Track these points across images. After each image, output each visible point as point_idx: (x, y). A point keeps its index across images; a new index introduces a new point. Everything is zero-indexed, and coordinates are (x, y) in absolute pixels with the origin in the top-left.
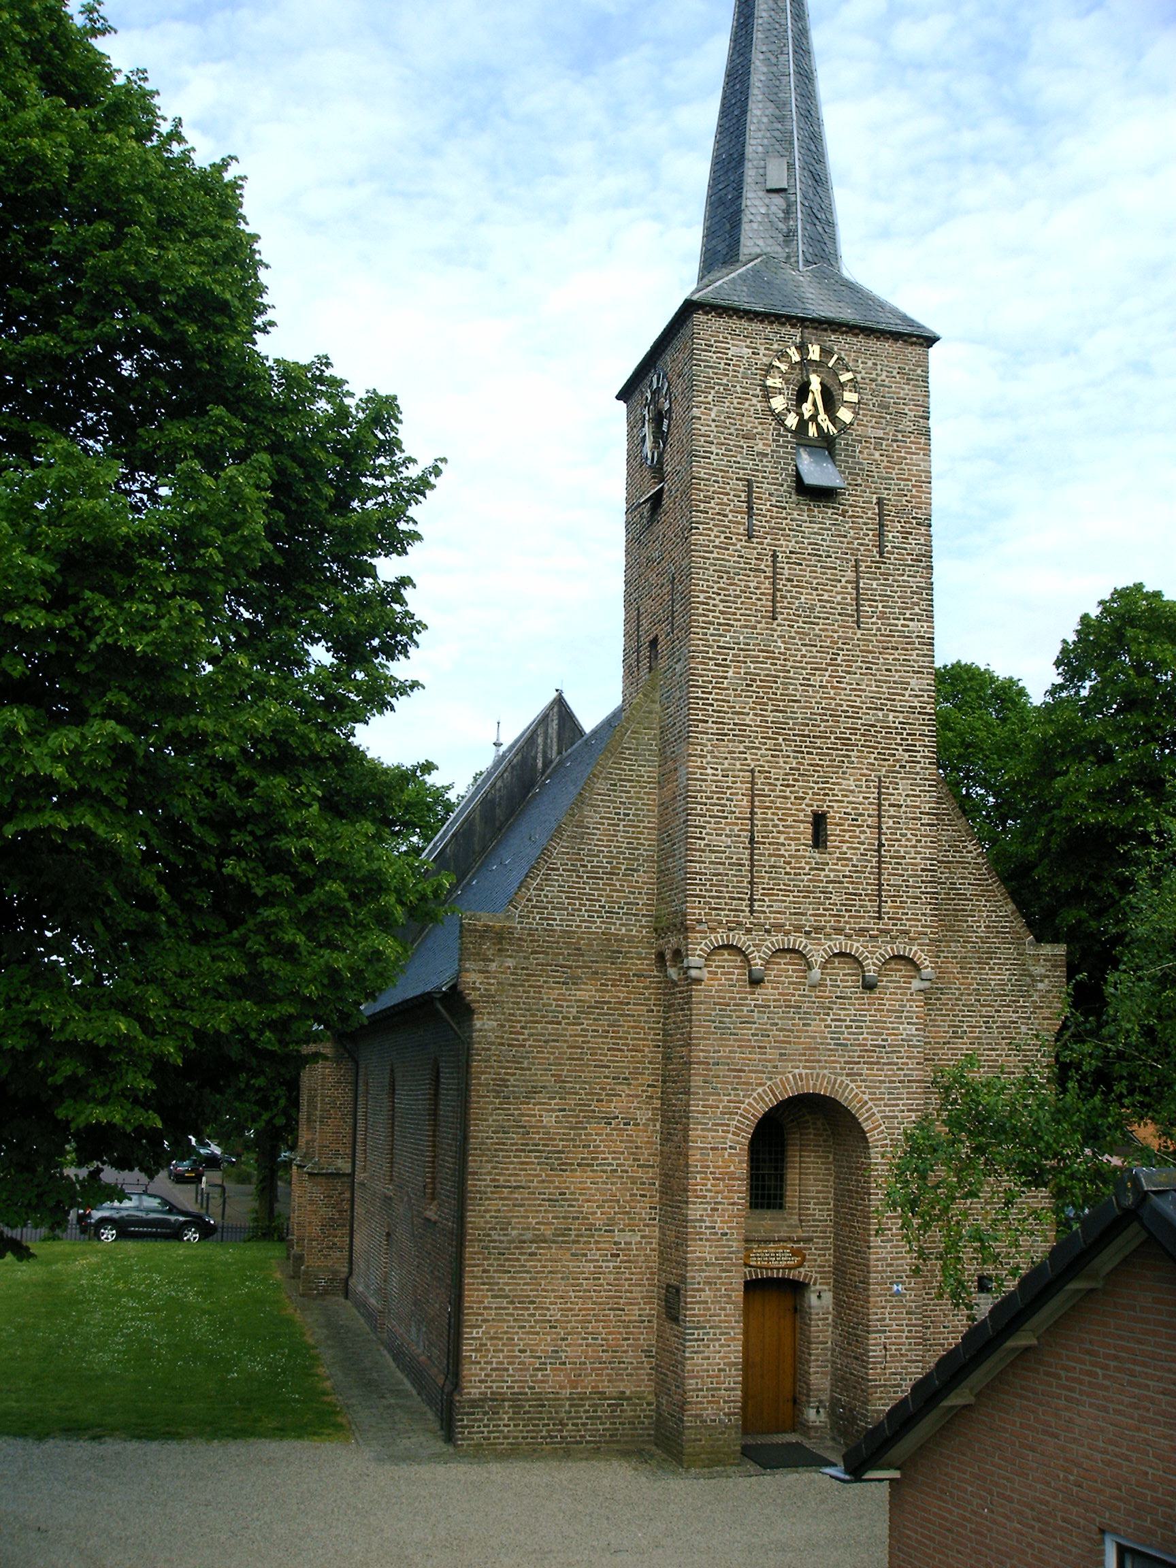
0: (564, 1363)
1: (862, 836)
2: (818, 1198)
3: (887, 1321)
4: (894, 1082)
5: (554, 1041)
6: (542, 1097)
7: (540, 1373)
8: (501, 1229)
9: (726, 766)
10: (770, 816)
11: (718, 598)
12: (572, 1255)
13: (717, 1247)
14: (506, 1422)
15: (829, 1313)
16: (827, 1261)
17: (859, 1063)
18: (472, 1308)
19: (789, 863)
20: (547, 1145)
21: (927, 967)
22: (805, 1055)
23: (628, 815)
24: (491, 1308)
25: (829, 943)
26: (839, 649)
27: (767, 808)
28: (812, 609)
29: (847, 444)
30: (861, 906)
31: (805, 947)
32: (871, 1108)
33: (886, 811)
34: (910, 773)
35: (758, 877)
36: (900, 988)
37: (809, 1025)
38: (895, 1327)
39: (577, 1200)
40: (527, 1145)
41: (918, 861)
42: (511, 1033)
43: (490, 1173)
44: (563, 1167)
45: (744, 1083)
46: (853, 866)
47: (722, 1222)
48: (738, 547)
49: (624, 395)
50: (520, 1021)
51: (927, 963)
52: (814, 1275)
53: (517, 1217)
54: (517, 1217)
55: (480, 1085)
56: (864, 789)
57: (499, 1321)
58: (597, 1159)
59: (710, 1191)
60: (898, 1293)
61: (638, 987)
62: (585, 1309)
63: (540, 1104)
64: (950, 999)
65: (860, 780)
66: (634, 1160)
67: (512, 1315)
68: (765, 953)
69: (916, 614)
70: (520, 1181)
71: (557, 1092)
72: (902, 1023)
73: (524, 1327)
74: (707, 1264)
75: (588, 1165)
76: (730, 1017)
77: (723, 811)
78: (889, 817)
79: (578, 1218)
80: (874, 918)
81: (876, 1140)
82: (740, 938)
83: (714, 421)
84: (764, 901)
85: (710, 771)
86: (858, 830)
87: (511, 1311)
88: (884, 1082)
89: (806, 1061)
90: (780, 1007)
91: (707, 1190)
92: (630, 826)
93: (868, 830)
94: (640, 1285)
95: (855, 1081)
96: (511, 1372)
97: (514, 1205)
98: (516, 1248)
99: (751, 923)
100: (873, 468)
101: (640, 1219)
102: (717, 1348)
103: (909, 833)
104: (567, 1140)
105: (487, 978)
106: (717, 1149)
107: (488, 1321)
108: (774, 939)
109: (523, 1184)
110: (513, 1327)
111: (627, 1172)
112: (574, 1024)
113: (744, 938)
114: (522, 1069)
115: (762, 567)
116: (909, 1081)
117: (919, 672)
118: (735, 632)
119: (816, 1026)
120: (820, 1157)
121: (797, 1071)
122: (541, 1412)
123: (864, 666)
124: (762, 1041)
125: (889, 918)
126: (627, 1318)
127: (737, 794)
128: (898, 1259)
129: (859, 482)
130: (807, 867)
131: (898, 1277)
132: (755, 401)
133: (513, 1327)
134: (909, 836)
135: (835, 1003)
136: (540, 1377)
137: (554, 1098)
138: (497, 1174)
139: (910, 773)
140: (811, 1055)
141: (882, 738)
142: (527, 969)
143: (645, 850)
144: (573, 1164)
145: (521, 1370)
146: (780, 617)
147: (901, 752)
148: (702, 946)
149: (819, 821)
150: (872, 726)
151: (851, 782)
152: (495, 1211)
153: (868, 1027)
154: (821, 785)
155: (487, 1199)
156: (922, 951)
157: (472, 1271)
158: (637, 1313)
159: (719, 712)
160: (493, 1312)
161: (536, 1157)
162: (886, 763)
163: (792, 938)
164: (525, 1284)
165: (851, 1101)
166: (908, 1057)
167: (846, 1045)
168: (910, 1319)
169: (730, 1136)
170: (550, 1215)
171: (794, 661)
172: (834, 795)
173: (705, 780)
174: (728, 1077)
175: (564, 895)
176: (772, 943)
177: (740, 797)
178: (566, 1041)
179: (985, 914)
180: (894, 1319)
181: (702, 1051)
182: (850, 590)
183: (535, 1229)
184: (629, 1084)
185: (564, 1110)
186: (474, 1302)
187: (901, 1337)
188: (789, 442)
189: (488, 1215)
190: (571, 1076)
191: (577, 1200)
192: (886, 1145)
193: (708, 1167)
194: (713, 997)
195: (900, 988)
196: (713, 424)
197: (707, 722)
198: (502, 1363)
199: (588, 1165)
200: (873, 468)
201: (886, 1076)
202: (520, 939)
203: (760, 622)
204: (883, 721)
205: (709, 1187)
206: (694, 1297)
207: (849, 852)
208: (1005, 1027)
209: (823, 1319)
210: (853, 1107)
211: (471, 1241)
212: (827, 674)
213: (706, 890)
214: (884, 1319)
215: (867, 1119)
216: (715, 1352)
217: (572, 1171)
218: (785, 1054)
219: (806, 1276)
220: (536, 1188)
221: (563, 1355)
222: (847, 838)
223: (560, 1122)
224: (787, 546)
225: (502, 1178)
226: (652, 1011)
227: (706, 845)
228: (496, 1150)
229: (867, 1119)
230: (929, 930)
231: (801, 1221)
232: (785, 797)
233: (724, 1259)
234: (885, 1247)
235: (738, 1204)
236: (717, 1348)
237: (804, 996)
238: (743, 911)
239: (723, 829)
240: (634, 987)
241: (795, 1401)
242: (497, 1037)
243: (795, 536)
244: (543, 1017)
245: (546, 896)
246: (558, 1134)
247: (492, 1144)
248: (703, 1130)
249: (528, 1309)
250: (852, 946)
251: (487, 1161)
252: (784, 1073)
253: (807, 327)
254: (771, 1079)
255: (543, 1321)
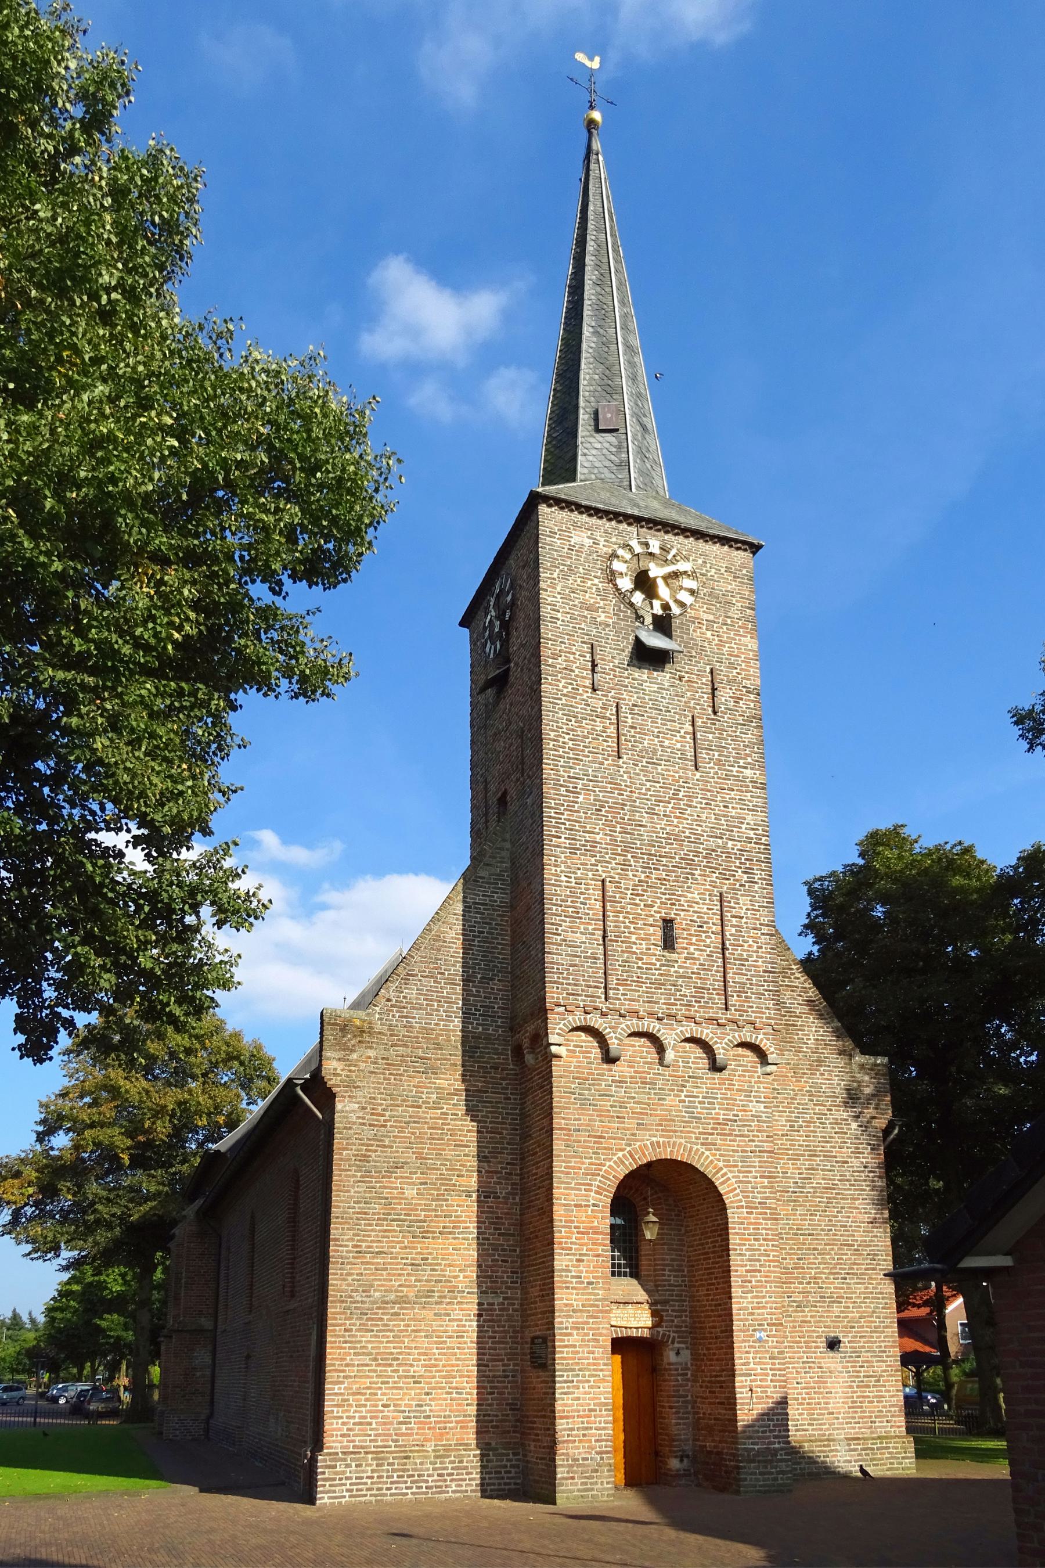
0: (429, 1417)
1: (708, 941)
2: (672, 1266)
3: (752, 1366)
4: (746, 1152)
5: (415, 1122)
6: (405, 1172)
7: (404, 1427)
8: (363, 1291)
9: (579, 875)
10: (621, 919)
11: (567, 737)
12: (435, 1314)
13: (583, 1294)
14: (369, 1474)
15: (688, 1369)
16: (683, 1321)
17: (712, 1134)
18: (334, 1365)
19: (641, 959)
20: (409, 1215)
21: (772, 1053)
22: (661, 1125)
23: (483, 932)
24: (354, 1365)
25: (681, 1028)
26: (680, 786)
27: (619, 912)
28: (655, 752)
29: (682, 623)
30: (710, 999)
31: (659, 1031)
32: (725, 1174)
33: (729, 921)
34: (749, 891)
35: (612, 970)
36: (748, 1071)
37: (664, 1099)
38: (759, 1371)
39: (440, 1264)
40: (390, 1214)
41: (760, 963)
42: (372, 1114)
43: (352, 1240)
44: (425, 1235)
45: (605, 1148)
46: (701, 964)
47: (587, 1272)
48: (585, 697)
49: (464, 623)
50: (381, 1104)
51: (772, 1049)
52: (672, 1335)
53: (380, 1280)
54: (380, 1280)
55: (341, 1160)
56: (707, 902)
57: (361, 1377)
58: (459, 1228)
59: (575, 1244)
60: (760, 1340)
61: (496, 1078)
62: (449, 1365)
63: (402, 1177)
64: (786, 1098)
65: (704, 894)
66: (495, 1229)
67: (376, 1371)
68: (620, 1034)
69: (749, 763)
70: (382, 1247)
71: (418, 1168)
72: (751, 1101)
73: (388, 1383)
74: (574, 1311)
75: (450, 1233)
76: (590, 1090)
77: (578, 913)
78: (732, 926)
79: (441, 1281)
80: (721, 1009)
81: (732, 1202)
82: (596, 1021)
83: (559, 593)
84: (618, 989)
85: (563, 878)
86: (704, 935)
87: (373, 1368)
88: (737, 1151)
89: (663, 1130)
90: (637, 1083)
91: (571, 1243)
92: (485, 942)
93: (713, 936)
94: (503, 1343)
95: (710, 1150)
96: (374, 1426)
97: (377, 1269)
98: (379, 1308)
99: (607, 1008)
100: (706, 644)
101: (502, 1282)
102: (587, 1389)
103: (750, 940)
104: (429, 1210)
105: (349, 1066)
106: (581, 1206)
107: (350, 1377)
108: (629, 1023)
109: (385, 1250)
110: (377, 1383)
111: (488, 1239)
112: (435, 1108)
113: (600, 1021)
114: (385, 1147)
115: (608, 715)
116: (760, 1152)
117: (753, 810)
118: (584, 765)
119: (670, 1100)
120: (671, 1229)
121: (654, 1139)
122: (405, 1464)
123: (704, 801)
124: (619, 1112)
125: (736, 1010)
126: (491, 1374)
127: (590, 899)
128: (759, 1308)
129: (694, 654)
130: (658, 963)
131: (759, 1325)
132: (596, 581)
133: (377, 1383)
134: (751, 943)
135: (688, 1081)
136: (404, 1431)
137: (416, 1173)
138: (358, 1241)
139: (749, 891)
140: (666, 1125)
141: (723, 861)
142: (387, 1059)
143: (499, 963)
144: (435, 1232)
145: (385, 1424)
146: (625, 757)
147: (740, 873)
148: (561, 1026)
149: (668, 924)
150: (713, 850)
151: (696, 896)
152: (357, 1274)
153: (719, 1104)
154: (668, 896)
155: (348, 1263)
156: (768, 1039)
157: (335, 1330)
158: (502, 1368)
159: (571, 830)
160: (356, 1368)
161: (398, 1226)
162: (727, 882)
163: (646, 1023)
164: (387, 1342)
165: (707, 1167)
166: (758, 1131)
167: (700, 1118)
168: (773, 1364)
169: (592, 1194)
170: (413, 1278)
171: (639, 793)
172: (680, 905)
173: (560, 886)
174: (590, 1142)
175: (422, 997)
176: (627, 1026)
177: (593, 901)
178: (426, 1123)
179: (814, 1029)
180: (759, 1364)
181: (564, 1118)
182: (688, 739)
183: (397, 1291)
184: (489, 1162)
185: (426, 1184)
186: (336, 1359)
187: (766, 1380)
188: (629, 617)
189: (350, 1278)
190: (432, 1154)
191: (440, 1264)
192: (742, 1207)
193: (572, 1222)
194: (572, 1072)
195: (748, 1071)
196: (559, 596)
197: (560, 837)
198: (365, 1417)
199: (450, 1233)
200: (706, 644)
201: (738, 1146)
202: (380, 1033)
203: (607, 760)
204: (724, 848)
205: (574, 1240)
206: (563, 1341)
207: (697, 953)
208: (836, 1123)
209: (682, 1375)
210: (709, 1172)
211: (334, 1302)
212: (670, 806)
213: (564, 978)
214: (748, 1363)
215: (723, 1183)
216: (586, 1393)
217: (433, 1238)
218: (642, 1124)
219: (664, 1335)
220: (399, 1253)
221: (427, 1408)
222: (694, 941)
223: (421, 1194)
224: (630, 700)
225: (364, 1244)
226: (509, 1099)
227: (562, 940)
228: (358, 1219)
229: (723, 1183)
230: (773, 1022)
231: (657, 1286)
232: (636, 905)
233: (591, 1306)
234: (746, 1298)
235: (603, 1256)
236: (587, 1389)
237: (659, 1074)
238: (599, 997)
239: (579, 928)
240: (492, 1078)
241: (657, 1454)
242: (359, 1118)
243: (637, 693)
244: (404, 1101)
245: (405, 997)
246: (420, 1205)
247: (354, 1213)
248: (566, 1188)
249: (391, 1365)
250: (702, 1032)
251: (348, 1229)
252: (642, 1140)
253: (642, 527)
254: (630, 1145)
255: (406, 1377)
